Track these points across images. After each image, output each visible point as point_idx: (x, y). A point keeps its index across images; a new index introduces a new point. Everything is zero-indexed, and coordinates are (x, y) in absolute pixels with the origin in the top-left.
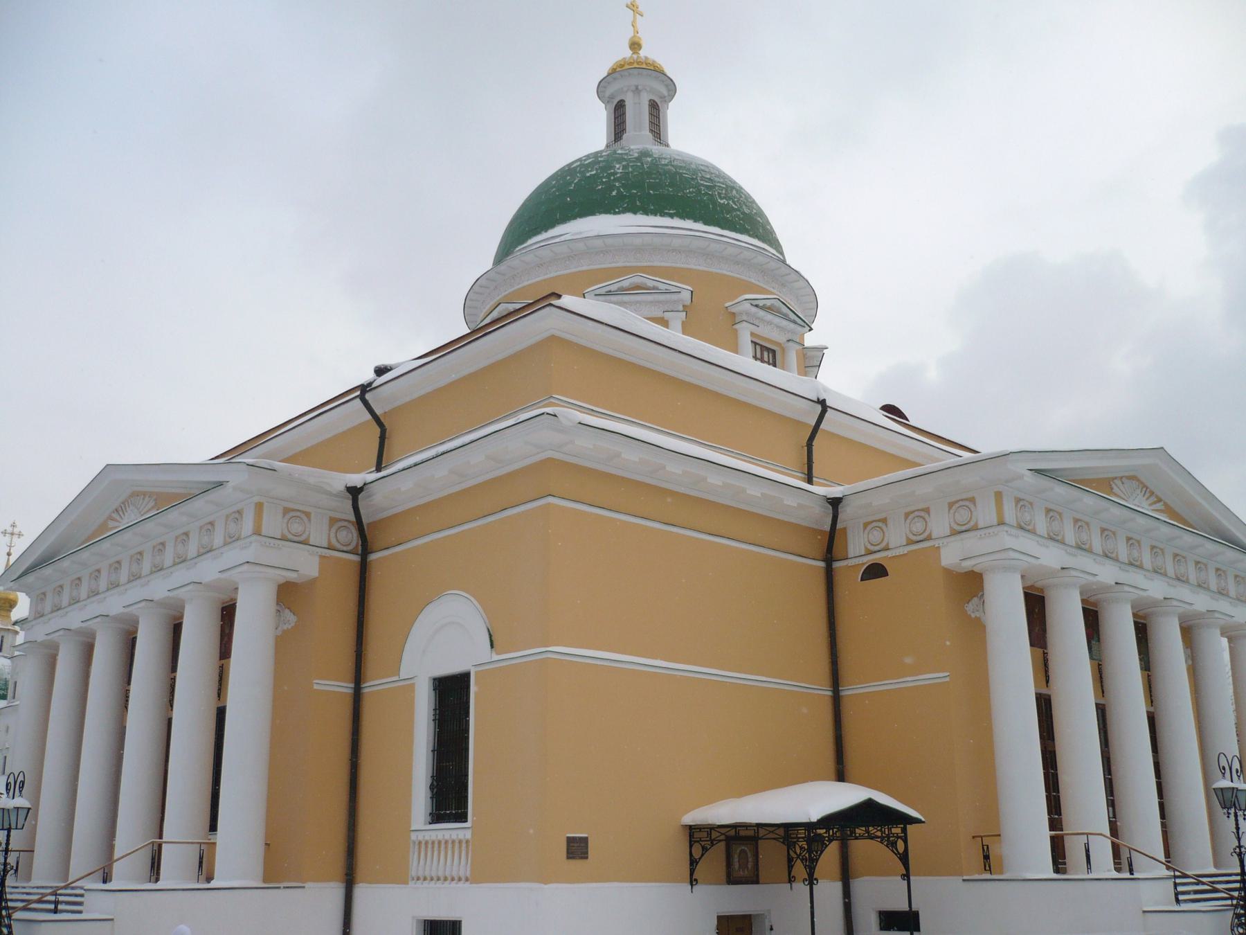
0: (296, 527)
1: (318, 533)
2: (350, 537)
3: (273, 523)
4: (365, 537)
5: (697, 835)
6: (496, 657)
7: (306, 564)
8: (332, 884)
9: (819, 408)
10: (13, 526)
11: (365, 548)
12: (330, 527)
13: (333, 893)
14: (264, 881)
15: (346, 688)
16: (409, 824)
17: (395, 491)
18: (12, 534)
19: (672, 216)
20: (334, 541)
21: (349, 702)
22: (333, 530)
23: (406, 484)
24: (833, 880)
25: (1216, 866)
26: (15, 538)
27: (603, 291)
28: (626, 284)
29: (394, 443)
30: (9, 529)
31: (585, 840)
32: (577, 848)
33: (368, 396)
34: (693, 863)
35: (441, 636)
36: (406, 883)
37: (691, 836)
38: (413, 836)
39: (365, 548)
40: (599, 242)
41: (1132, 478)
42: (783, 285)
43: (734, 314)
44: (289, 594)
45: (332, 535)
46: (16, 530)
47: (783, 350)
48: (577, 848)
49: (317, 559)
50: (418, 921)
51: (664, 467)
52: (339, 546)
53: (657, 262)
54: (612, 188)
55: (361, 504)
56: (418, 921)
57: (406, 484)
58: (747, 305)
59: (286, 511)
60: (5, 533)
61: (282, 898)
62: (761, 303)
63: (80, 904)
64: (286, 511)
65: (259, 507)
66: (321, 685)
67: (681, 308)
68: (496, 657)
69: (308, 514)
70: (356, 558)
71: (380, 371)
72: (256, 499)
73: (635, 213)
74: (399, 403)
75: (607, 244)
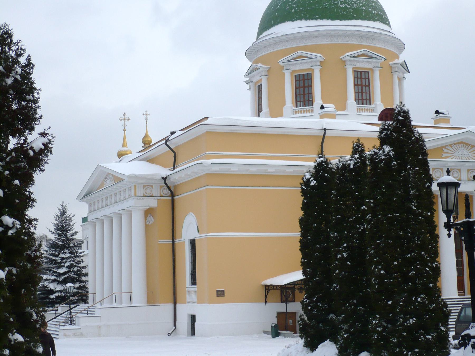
0: (148, 191)
1: (156, 192)
2: (167, 191)
3: (140, 192)
4: (171, 191)
5: (267, 288)
6: (199, 235)
7: (153, 203)
8: (169, 304)
9: (323, 131)
10: (125, 115)
11: (173, 195)
12: (160, 189)
13: (171, 306)
14: (148, 304)
15: (170, 241)
16: (185, 286)
17: (178, 176)
18: (125, 119)
19: (316, 19)
20: (162, 194)
21: (171, 246)
22: (161, 190)
23: (182, 175)
24: (166, 302)
25: (459, 295)
26: (126, 121)
27: (286, 60)
28: (295, 56)
29: (179, 158)
30: (123, 117)
31: (223, 291)
32: (220, 293)
33: (168, 143)
34: (266, 296)
35: (189, 229)
36: (186, 303)
37: (265, 288)
38: (187, 289)
39: (173, 195)
40: (284, 37)
41: (461, 143)
42: (373, 39)
43: (345, 61)
44: (149, 212)
45: (161, 192)
46: (126, 117)
47: (293, 72)
48: (220, 293)
49: (156, 201)
50: (189, 315)
51: (249, 170)
52: (164, 195)
53: (309, 43)
54: (292, 7)
55: (167, 182)
56: (189, 315)
57: (182, 175)
58: (349, 58)
59: (144, 186)
60: (121, 119)
61: (153, 309)
62: (356, 55)
63: (94, 311)
64: (144, 186)
65: (135, 186)
66: (161, 242)
67: (318, 64)
68: (199, 235)
69: (152, 186)
70: (171, 198)
71: (172, 133)
72: (134, 184)
73: (301, 20)
74: (179, 144)
75: (287, 38)
